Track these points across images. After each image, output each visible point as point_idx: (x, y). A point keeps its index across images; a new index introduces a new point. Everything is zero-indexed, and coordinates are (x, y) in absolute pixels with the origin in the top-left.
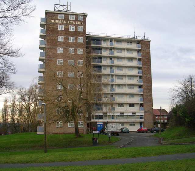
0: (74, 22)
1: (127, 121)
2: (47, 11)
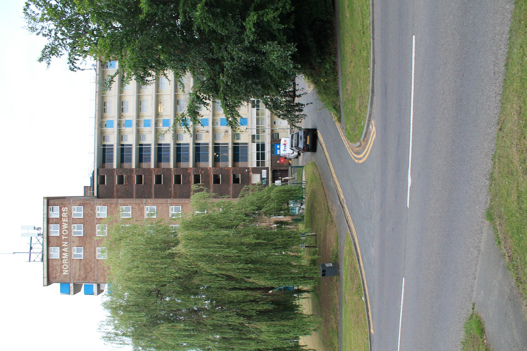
0: (65, 226)
1: (270, 118)
2: (46, 283)
